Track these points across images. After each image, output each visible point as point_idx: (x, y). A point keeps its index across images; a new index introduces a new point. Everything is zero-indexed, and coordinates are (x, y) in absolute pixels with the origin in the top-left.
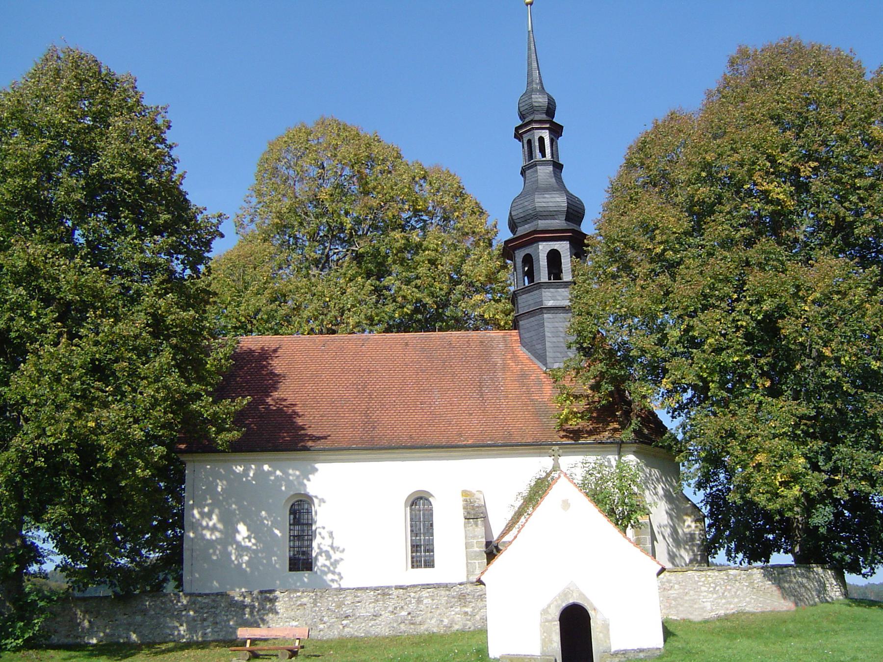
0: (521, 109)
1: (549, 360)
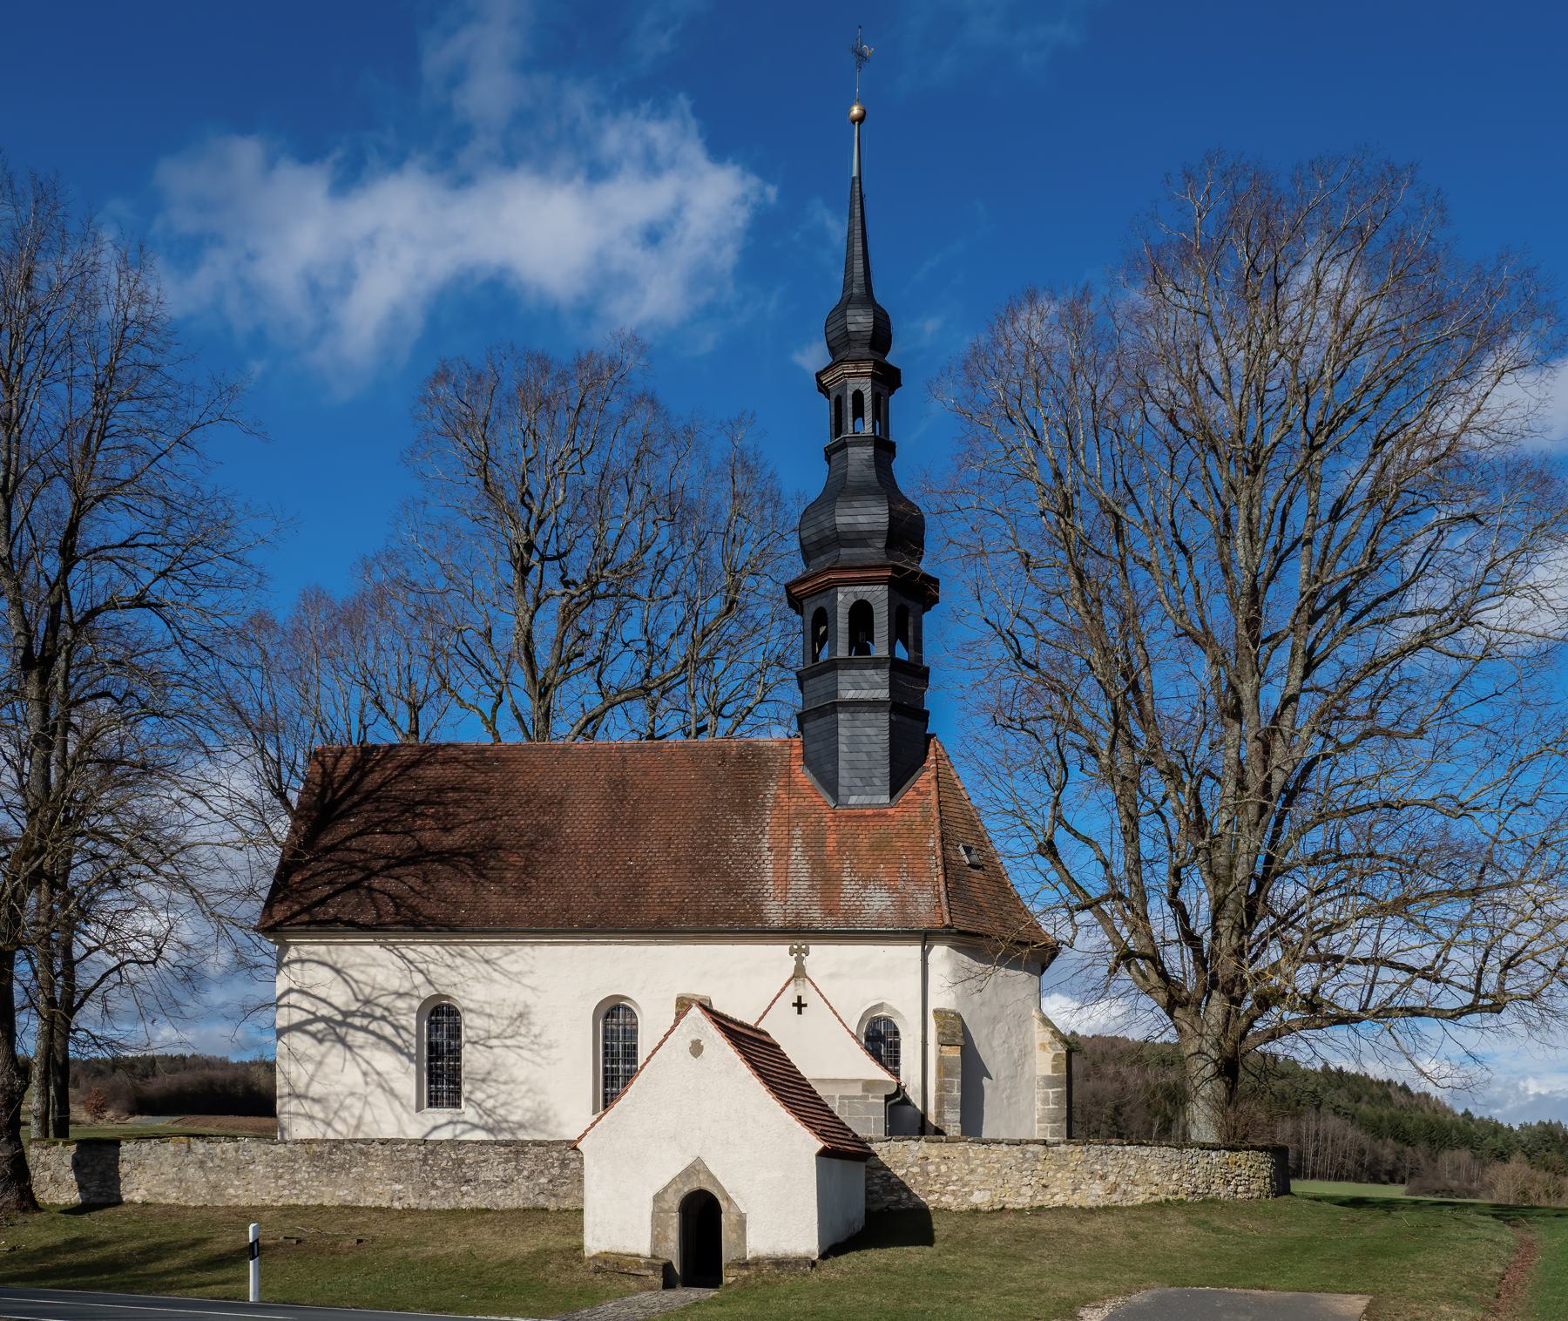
0: (831, 337)
1: (841, 790)
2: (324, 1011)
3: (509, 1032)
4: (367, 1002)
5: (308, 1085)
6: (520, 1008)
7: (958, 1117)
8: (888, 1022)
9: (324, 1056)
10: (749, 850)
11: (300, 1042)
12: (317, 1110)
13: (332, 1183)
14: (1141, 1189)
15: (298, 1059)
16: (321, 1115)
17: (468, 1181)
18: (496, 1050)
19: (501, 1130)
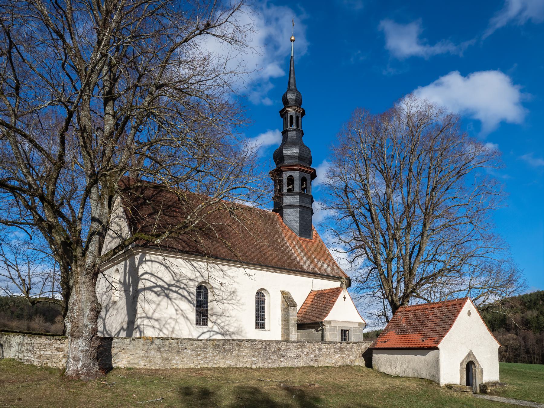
2: (160, 283)
3: (229, 298)
4: (178, 281)
5: (153, 314)
6: (233, 290)
9: (160, 302)
11: (150, 295)
12: (156, 324)
13: (224, 357)
15: (149, 302)
16: (158, 326)
17: (283, 357)
18: (225, 305)
19: (226, 335)
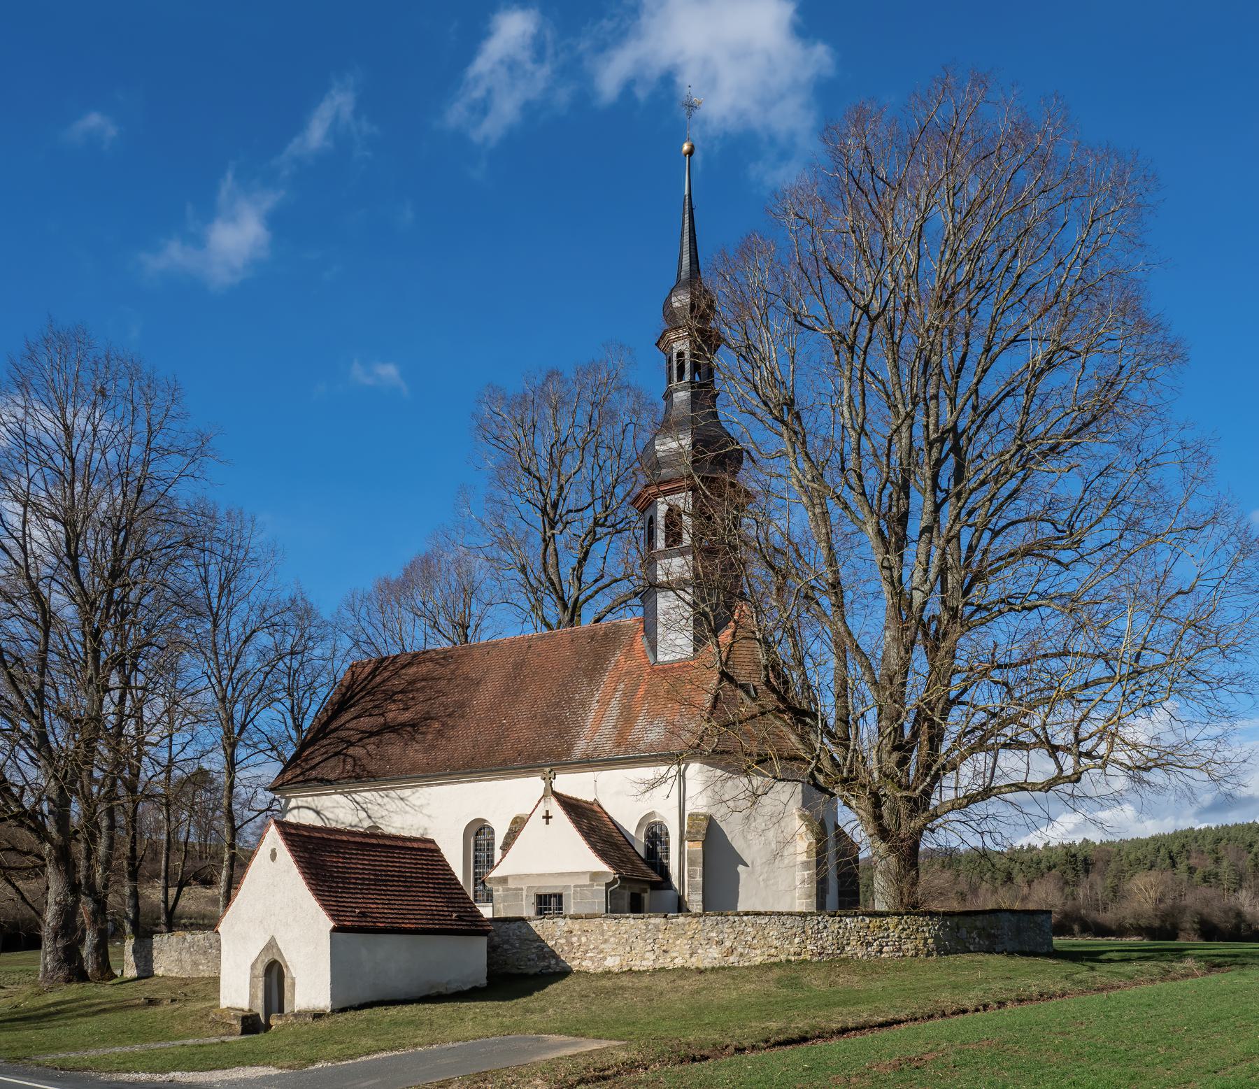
7: (700, 898)
8: (661, 824)
10: (583, 704)
14: (758, 952)
